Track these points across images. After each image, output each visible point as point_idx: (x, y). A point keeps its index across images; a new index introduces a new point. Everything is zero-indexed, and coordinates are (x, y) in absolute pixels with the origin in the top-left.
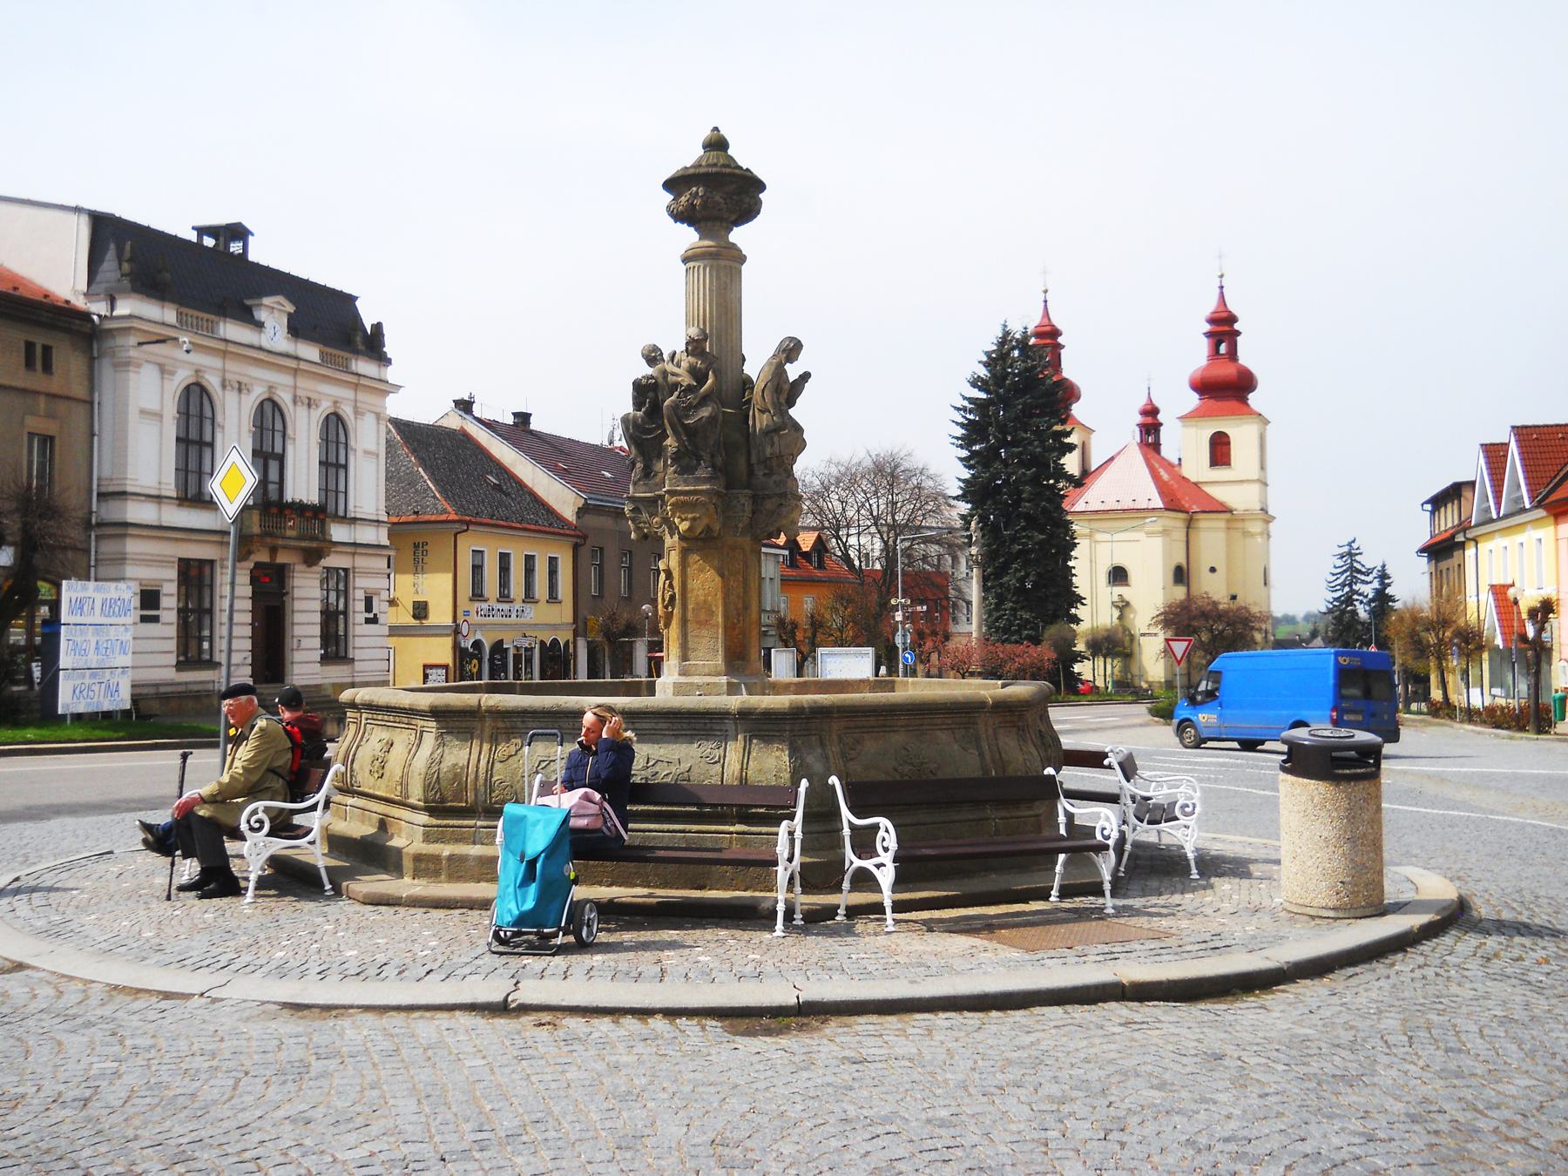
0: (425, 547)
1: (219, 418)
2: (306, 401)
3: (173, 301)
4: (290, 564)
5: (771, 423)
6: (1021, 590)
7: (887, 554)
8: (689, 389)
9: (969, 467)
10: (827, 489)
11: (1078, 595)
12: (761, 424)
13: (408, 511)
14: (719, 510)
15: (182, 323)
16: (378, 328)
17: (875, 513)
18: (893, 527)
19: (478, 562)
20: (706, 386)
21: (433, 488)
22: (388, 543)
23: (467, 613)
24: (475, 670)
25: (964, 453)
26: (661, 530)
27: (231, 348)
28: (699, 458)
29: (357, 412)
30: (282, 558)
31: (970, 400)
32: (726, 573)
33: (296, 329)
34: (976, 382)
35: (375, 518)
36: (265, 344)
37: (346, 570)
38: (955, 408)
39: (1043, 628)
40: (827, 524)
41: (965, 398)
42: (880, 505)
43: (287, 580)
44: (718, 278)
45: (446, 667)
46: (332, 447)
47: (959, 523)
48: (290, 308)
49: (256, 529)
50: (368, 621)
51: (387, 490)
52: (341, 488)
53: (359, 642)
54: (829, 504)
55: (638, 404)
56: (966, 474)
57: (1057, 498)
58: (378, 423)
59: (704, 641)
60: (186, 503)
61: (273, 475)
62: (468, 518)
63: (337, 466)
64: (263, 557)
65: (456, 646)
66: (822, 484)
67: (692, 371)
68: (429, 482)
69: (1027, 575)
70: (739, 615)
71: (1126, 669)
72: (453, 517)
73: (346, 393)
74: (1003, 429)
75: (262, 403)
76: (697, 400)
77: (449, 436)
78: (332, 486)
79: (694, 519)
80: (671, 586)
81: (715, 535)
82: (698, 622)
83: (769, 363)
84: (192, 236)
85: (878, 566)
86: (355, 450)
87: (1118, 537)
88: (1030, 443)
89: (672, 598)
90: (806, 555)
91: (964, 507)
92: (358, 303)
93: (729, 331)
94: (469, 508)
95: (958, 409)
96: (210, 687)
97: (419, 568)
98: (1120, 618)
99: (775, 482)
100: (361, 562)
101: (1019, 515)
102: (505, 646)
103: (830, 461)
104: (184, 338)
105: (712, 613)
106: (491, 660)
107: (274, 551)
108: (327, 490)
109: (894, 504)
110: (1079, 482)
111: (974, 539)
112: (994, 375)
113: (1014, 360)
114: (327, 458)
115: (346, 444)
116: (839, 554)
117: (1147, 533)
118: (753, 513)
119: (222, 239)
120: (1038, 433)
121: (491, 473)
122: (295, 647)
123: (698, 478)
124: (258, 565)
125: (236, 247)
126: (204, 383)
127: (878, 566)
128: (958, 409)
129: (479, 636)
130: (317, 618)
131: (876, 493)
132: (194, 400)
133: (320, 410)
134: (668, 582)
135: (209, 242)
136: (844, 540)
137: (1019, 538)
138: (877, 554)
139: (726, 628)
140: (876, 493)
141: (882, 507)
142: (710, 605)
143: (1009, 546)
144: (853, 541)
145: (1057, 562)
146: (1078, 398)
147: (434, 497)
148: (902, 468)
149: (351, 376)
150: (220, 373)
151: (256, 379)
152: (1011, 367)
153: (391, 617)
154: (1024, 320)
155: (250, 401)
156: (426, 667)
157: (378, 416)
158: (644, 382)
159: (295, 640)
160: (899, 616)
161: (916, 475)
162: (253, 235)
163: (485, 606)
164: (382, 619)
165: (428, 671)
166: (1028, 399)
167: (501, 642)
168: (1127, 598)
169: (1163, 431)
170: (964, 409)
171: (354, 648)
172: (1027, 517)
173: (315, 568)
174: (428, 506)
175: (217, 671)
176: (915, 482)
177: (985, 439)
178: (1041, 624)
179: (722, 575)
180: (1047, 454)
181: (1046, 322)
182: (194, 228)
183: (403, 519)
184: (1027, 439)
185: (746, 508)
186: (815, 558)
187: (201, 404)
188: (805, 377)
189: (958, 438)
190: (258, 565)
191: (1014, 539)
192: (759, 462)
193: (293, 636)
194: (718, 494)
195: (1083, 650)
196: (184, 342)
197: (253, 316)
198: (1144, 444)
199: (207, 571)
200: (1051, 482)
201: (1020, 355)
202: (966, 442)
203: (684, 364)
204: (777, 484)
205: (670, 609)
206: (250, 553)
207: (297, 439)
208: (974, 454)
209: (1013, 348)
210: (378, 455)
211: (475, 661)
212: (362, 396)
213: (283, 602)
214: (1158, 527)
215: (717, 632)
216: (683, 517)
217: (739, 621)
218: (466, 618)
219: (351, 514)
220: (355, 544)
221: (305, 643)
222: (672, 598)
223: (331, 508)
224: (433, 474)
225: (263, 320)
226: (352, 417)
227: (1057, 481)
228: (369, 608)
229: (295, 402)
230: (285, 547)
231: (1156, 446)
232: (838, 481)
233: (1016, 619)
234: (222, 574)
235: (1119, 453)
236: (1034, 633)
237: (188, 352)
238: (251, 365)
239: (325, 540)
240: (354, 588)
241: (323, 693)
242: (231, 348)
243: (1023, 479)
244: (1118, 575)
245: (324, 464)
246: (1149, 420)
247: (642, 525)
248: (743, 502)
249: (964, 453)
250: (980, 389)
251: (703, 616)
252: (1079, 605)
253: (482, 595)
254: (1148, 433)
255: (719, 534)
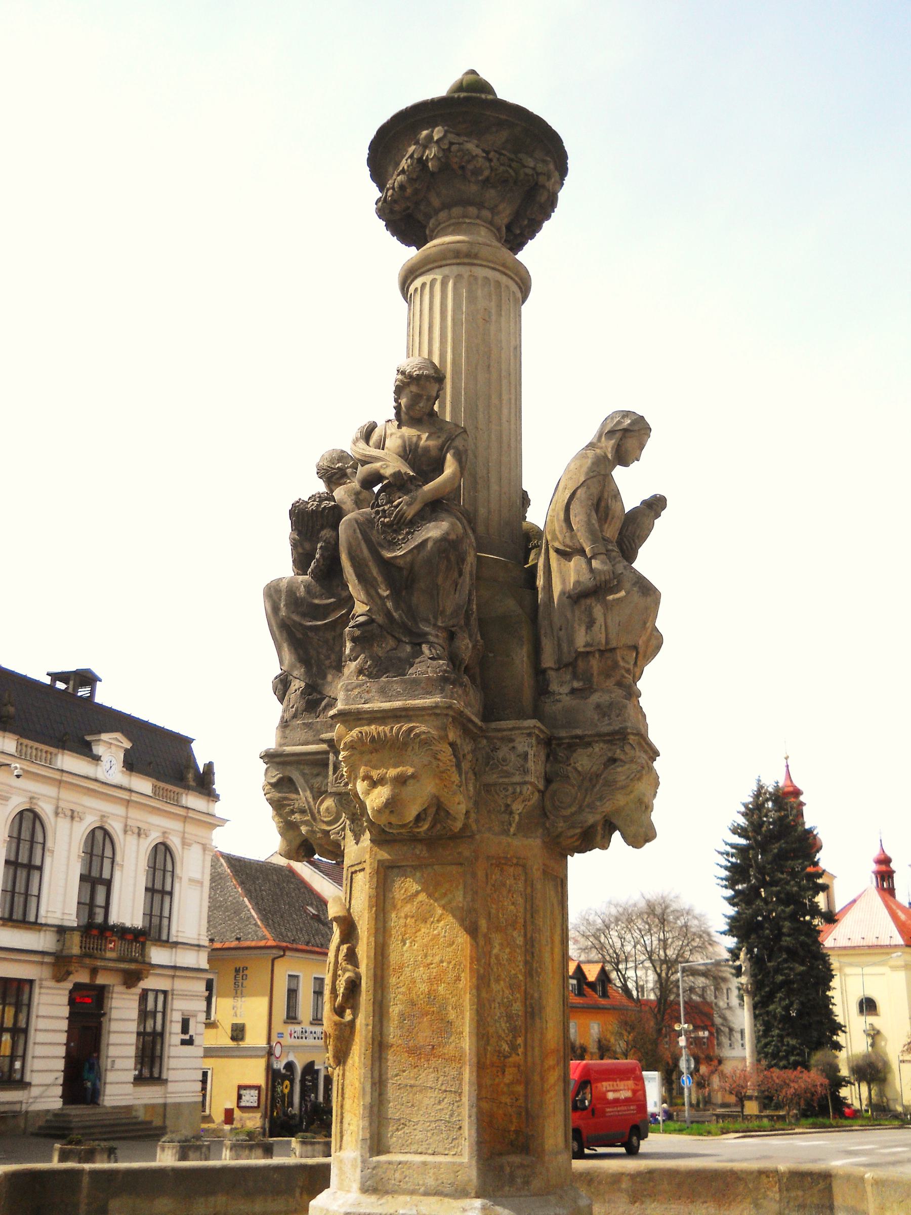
0: (245, 972)
1: (49, 844)
2: (136, 831)
3: (14, 732)
4: (109, 986)
5: (586, 577)
6: (786, 1018)
7: (661, 984)
8: (398, 484)
9: (734, 905)
10: (608, 927)
11: (839, 1024)
12: (564, 582)
13: (231, 938)
14: (465, 766)
15: (20, 755)
16: (209, 767)
17: (649, 949)
18: (666, 961)
19: (293, 987)
20: (431, 485)
21: (256, 916)
22: (207, 966)
23: (281, 1035)
24: (286, 1091)
25: (730, 893)
26: (336, 827)
27: (66, 778)
28: (418, 640)
29: (185, 843)
30: (100, 980)
31: (733, 846)
32: (483, 923)
33: (131, 764)
34: (737, 830)
35: (196, 942)
36: (101, 776)
37: (165, 993)
38: (719, 852)
39: (809, 1054)
40: (608, 958)
41: (727, 844)
42: (652, 941)
43: (105, 1001)
44: (472, 299)
45: (258, 1088)
46: (159, 874)
47: (726, 955)
48: (128, 745)
49: (76, 950)
50: (184, 1042)
51: (209, 917)
52: (166, 914)
53: (173, 1063)
54: (610, 940)
55: (301, 562)
56: (732, 911)
57: (814, 934)
58: (204, 854)
59: (428, 1100)
60: (10, 924)
61: (100, 900)
62: (284, 944)
63: (163, 892)
64: (83, 978)
65: (269, 1067)
66: (604, 922)
67: (409, 453)
68: (252, 911)
69: (791, 1004)
70: (514, 1030)
71: (881, 1094)
72: (271, 943)
73: (174, 825)
74: (761, 870)
75: (93, 831)
76: (416, 507)
77: (275, 871)
78: (156, 911)
79: (401, 781)
80: (352, 957)
81: (459, 825)
82: (413, 1051)
83: (581, 456)
84: (47, 680)
85: (652, 997)
86: (181, 878)
87: (867, 970)
88: (787, 883)
89: (353, 986)
90: (592, 985)
91: (731, 942)
92: (193, 745)
93: (494, 400)
94: (287, 935)
95: (722, 854)
96: (17, 1108)
97: (239, 992)
98: (873, 1045)
99: (598, 706)
100: (180, 985)
101: (781, 949)
102: (316, 1068)
103: (610, 903)
104: (17, 765)
105: (445, 1027)
106: (303, 1081)
107: (94, 972)
108: (151, 915)
109: (665, 940)
110: (831, 918)
111: (743, 969)
112: (751, 823)
113: (769, 810)
114: (153, 885)
115: (44, 844)
116: (619, 984)
117: (891, 967)
118: (548, 781)
119: (71, 683)
120: (793, 874)
121: (311, 905)
122: (109, 1067)
123: (415, 682)
124: (77, 987)
125: (83, 692)
126: (38, 810)
127: (652, 997)
128: (722, 854)
129: (291, 1058)
130: (133, 1039)
131: (650, 930)
132: (26, 825)
133: (149, 839)
134: (344, 948)
135: (60, 685)
136: (623, 973)
137: (783, 969)
138: (651, 985)
139: (481, 1067)
140: (650, 930)
141: (655, 943)
142: (443, 1007)
143: (773, 977)
144: (630, 973)
145: (817, 992)
146: (821, 848)
147: (256, 925)
148: (672, 909)
149: (181, 809)
150: (54, 801)
151: (90, 808)
152: (766, 816)
153: (206, 1038)
154: (773, 779)
155: (81, 830)
156: (240, 1087)
157: (205, 848)
158: (312, 506)
159: (109, 1060)
160: (682, 1042)
161: (683, 915)
162: (100, 681)
163: (298, 1028)
164: (197, 1040)
165: (242, 1092)
166: (782, 843)
167: (312, 1064)
168: (877, 1026)
169: (896, 877)
170: (727, 854)
171: (168, 1069)
172: (788, 950)
173: (133, 990)
174: (249, 933)
175: (26, 1092)
176: (683, 921)
177: (745, 878)
178: (807, 1050)
179: (472, 930)
180: (803, 893)
181: (789, 783)
182: (48, 674)
183: (227, 945)
184: (783, 879)
185: (531, 764)
186: (599, 988)
187: (165, 856)
188: (655, 505)
189: (722, 879)
190: (77, 987)
191: (778, 970)
192: (561, 666)
193: (107, 1057)
194: (460, 720)
195: (848, 1075)
196: (16, 768)
197: (91, 750)
198: (880, 889)
199: (26, 989)
200: (808, 918)
201: (773, 806)
202: (731, 882)
203: (393, 443)
204: (603, 711)
205: (348, 1016)
206: (69, 973)
207: (125, 864)
208: (738, 893)
209: (767, 800)
210: (202, 883)
211: (287, 1083)
212: (191, 829)
213: (100, 1023)
214: (901, 962)
215: (459, 1078)
216: (375, 774)
217: (514, 1047)
218: (281, 1040)
219: (173, 939)
220: (175, 968)
221: (119, 1064)
222: (353, 986)
223: (153, 933)
224: (257, 904)
225: (100, 754)
226: (179, 846)
227: (813, 917)
228: (185, 1029)
229: (125, 832)
230: (106, 969)
231: (891, 891)
232: (617, 920)
233: (783, 1045)
234: (40, 994)
235: (860, 896)
236: (800, 1059)
237: (18, 776)
238: (85, 794)
239: (144, 962)
240: (172, 1010)
241: (134, 1114)
242: (66, 778)
243: (783, 915)
244: (868, 1006)
245: (150, 890)
246: (883, 868)
247: (297, 817)
248: (521, 748)
249: (730, 893)
250: (740, 835)
251: (424, 1036)
252: (840, 1033)
253: (295, 1018)
254: (883, 880)
255: (465, 826)
